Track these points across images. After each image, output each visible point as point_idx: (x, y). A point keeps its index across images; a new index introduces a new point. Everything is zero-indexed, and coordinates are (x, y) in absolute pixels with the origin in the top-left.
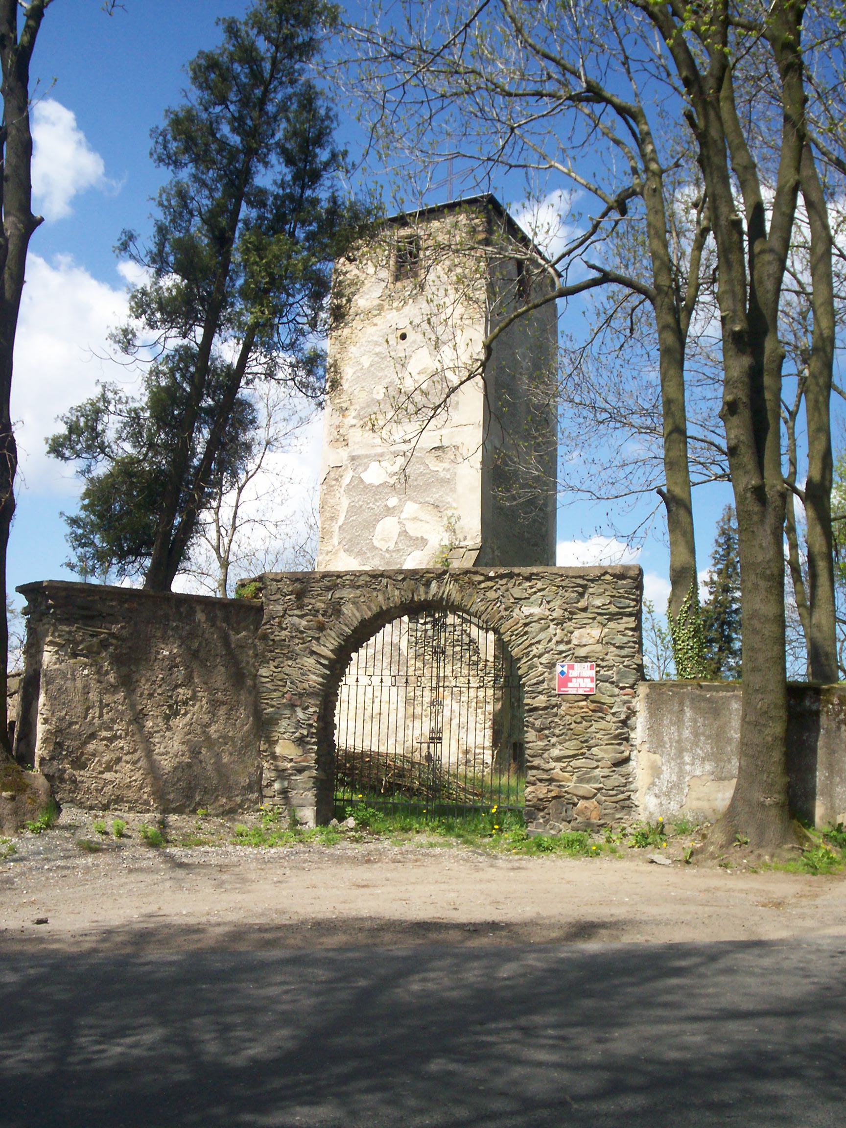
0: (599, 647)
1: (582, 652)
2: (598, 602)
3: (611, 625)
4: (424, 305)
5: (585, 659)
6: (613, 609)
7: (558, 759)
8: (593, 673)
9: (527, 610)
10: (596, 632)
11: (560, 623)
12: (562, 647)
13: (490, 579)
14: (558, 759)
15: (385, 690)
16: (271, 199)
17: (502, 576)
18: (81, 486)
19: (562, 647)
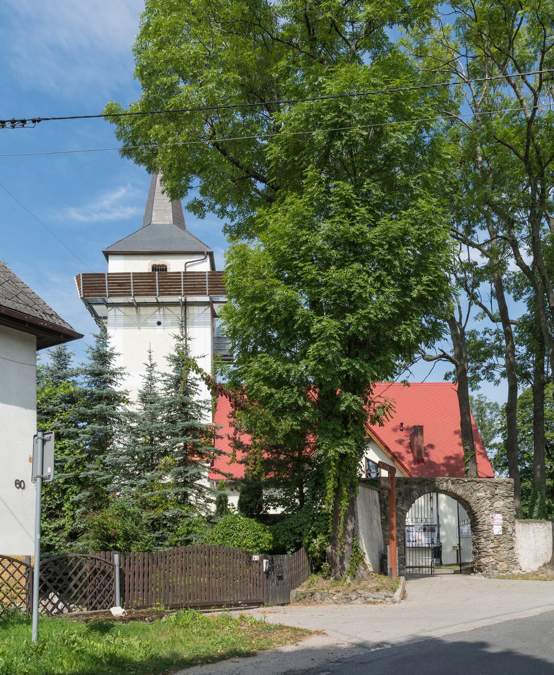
0: (503, 508)
1: (497, 510)
2: (502, 492)
3: (506, 500)
4: (461, 131)
5: (499, 512)
6: (506, 495)
7: (492, 548)
8: (501, 517)
9: (478, 495)
10: (502, 503)
11: (489, 499)
12: (491, 508)
13: (465, 482)
14: (492, 548)
15: (420, 517)
16: (483, 377)
17: (469, 481)
18: (525, 305)
19: (491, 508)
